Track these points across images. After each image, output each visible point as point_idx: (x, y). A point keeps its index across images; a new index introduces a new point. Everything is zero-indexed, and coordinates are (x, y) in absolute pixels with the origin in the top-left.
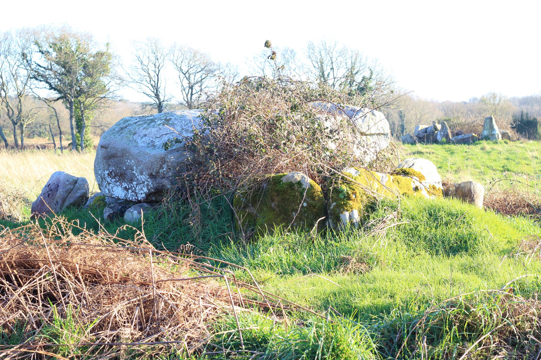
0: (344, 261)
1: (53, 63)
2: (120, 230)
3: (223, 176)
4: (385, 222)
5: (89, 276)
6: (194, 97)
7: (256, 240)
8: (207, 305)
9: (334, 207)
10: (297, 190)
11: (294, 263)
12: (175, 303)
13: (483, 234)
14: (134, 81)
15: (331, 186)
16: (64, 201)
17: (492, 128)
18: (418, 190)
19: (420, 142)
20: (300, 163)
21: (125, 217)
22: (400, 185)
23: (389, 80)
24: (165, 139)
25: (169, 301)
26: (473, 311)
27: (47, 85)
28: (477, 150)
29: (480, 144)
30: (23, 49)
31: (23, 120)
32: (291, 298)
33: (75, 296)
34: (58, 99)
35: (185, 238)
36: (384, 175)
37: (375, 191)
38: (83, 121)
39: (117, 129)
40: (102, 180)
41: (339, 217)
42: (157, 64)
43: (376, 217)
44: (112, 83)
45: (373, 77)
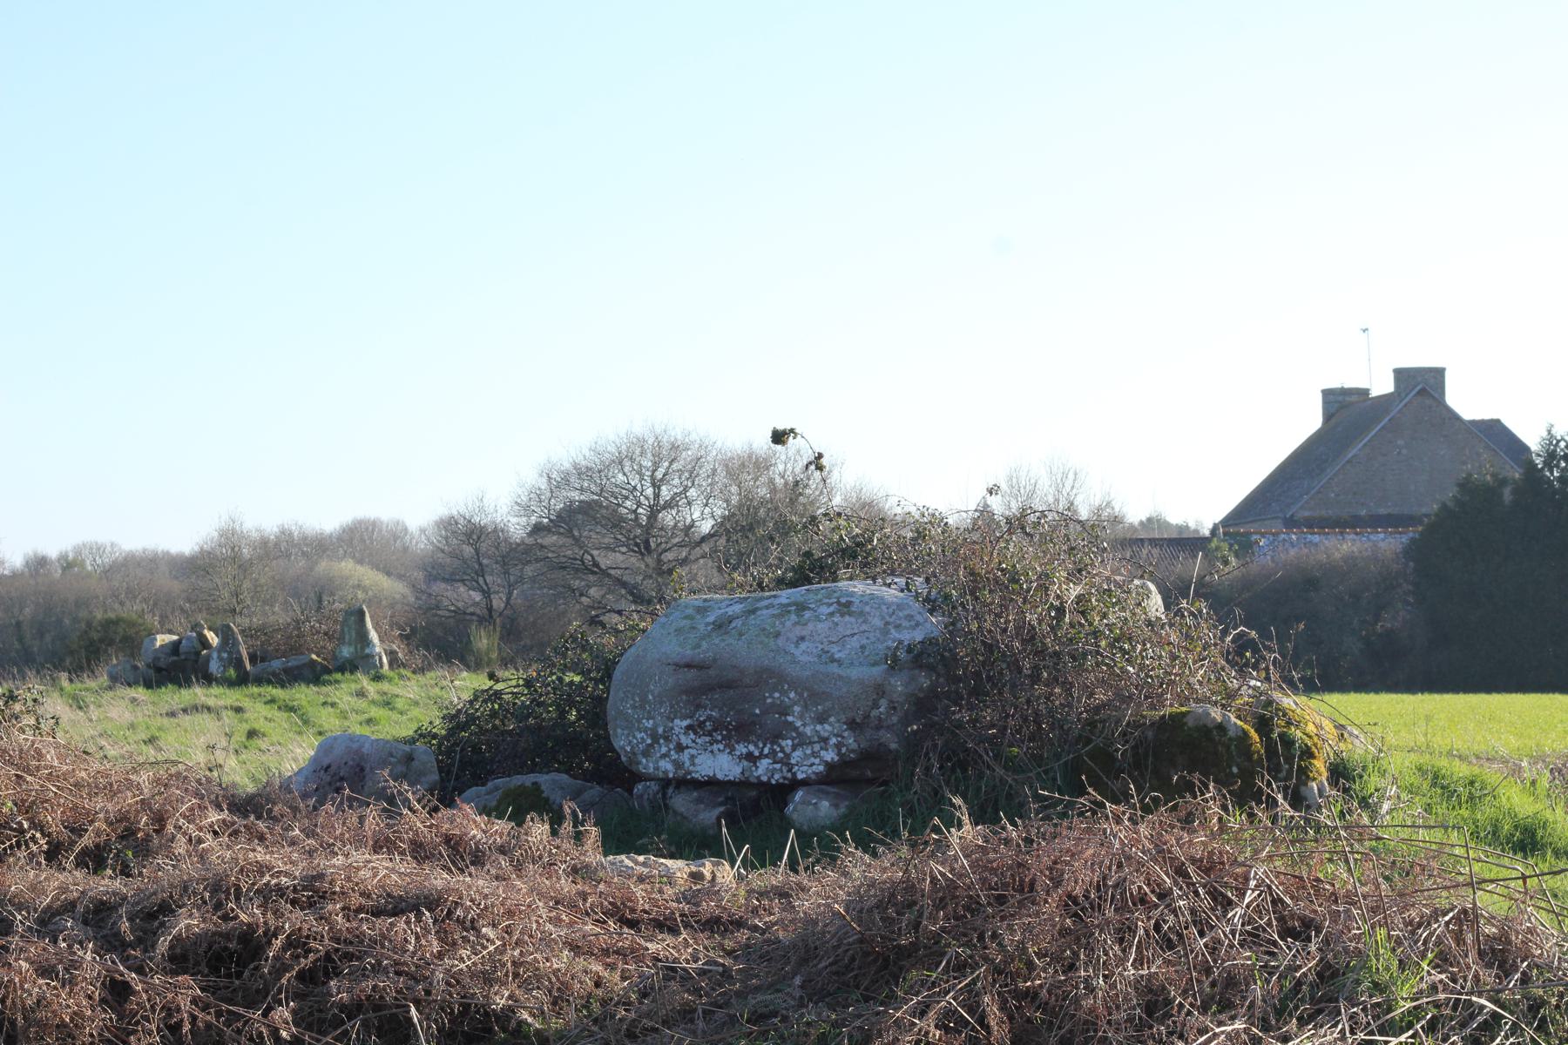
17: (363, 638)
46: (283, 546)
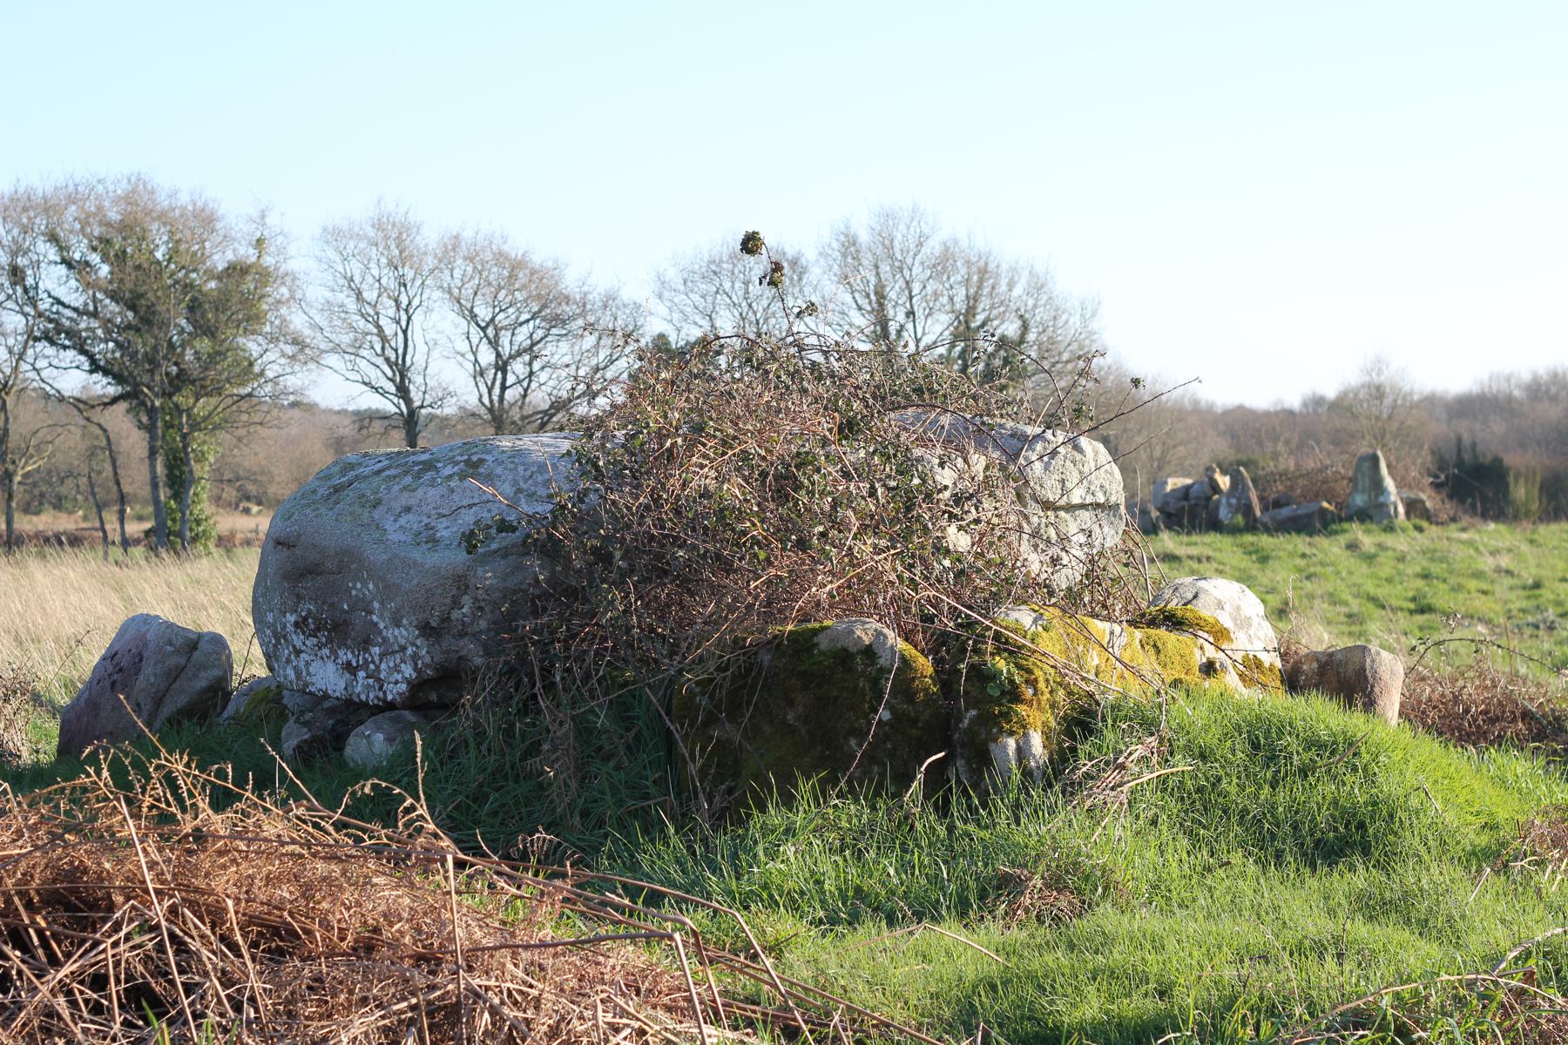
0: (1008, 885)
1: (99, 296)
2: (353, 793)
3: (642, 630)
4: (1122, 767)
5: (260, 934)
6: (509, 394)
7: (741, 822)
8: (617, 1020)
9: (972, 721)
10: (864, 671)
11: (858, 890)
12: (521, 1015)
13: (1414, 802)
14: (337, 348)
15: (962, 661)
16: (158, 702)
17: (1377, 486)
18: (1215, 671)
19: (1169, 528)
20: (869, 593)
21: (348, 751)
22: (1162, 656)
23: (1074, 346)
24: (467, 519)
25: (506, 1010)
26: (1420, 1039)
27: (83, 358)
28: (1336, 550)
29: (1344, 531)
30: (14, 254)
31: (14, 462)
32: (863, 996)
33: (222, 994)
34: (115, 400)
35: (530, 813)
36: (1117, 628)
37: (1091, 676)
38: (188, 463)
39: (321, 491)
40: (278, 642)
41: (987, 752)
42: (404, 300)
43: (1096, 754)
44: (270, 356)
45: (1031, 337)
46: (1554, 390)
